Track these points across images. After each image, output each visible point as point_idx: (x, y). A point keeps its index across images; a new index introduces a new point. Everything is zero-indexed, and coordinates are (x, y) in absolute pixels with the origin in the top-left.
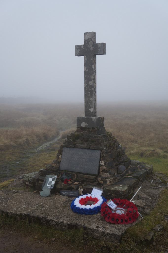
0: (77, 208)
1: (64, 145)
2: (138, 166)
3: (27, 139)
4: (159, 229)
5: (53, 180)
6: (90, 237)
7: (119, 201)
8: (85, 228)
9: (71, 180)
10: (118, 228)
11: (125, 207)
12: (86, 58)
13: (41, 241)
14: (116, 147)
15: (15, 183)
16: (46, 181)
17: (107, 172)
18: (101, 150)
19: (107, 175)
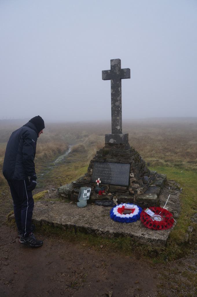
0: (118, 217)
1: (94, 159)
2: (155, 176)
3: (45, 154)
4: (191, 230)
5: (88, 191)
6: (137, 244)
7: (155, 209)
8: (132, 236)
9: (105, 191)
10: (161, 234)
11: (160, 214)
12: (113, 81)
13: (90, 248)
14: (140, 160)
15: (50, 195)
16: (81, 193)
17: (137, 183)
18: (130, 164)
19: (137, 185)
